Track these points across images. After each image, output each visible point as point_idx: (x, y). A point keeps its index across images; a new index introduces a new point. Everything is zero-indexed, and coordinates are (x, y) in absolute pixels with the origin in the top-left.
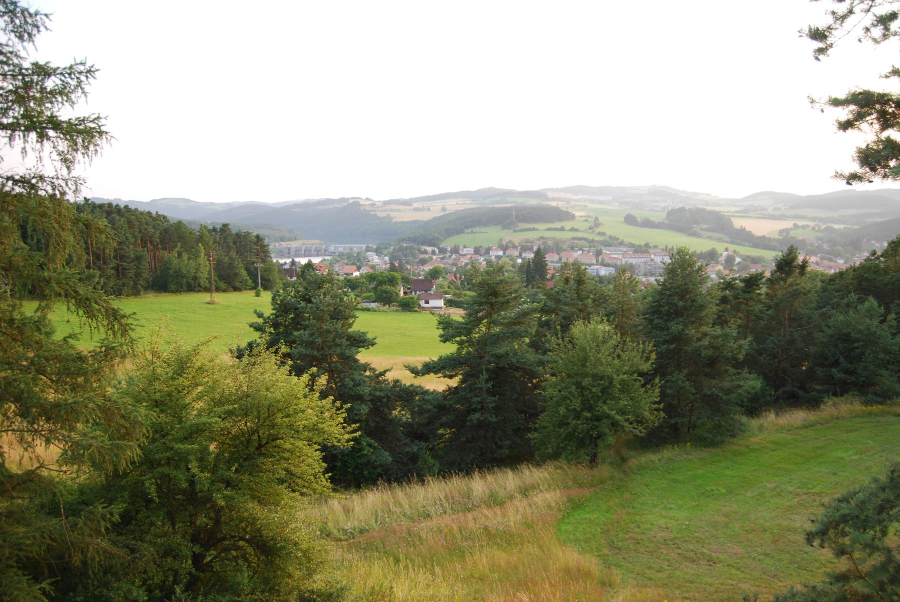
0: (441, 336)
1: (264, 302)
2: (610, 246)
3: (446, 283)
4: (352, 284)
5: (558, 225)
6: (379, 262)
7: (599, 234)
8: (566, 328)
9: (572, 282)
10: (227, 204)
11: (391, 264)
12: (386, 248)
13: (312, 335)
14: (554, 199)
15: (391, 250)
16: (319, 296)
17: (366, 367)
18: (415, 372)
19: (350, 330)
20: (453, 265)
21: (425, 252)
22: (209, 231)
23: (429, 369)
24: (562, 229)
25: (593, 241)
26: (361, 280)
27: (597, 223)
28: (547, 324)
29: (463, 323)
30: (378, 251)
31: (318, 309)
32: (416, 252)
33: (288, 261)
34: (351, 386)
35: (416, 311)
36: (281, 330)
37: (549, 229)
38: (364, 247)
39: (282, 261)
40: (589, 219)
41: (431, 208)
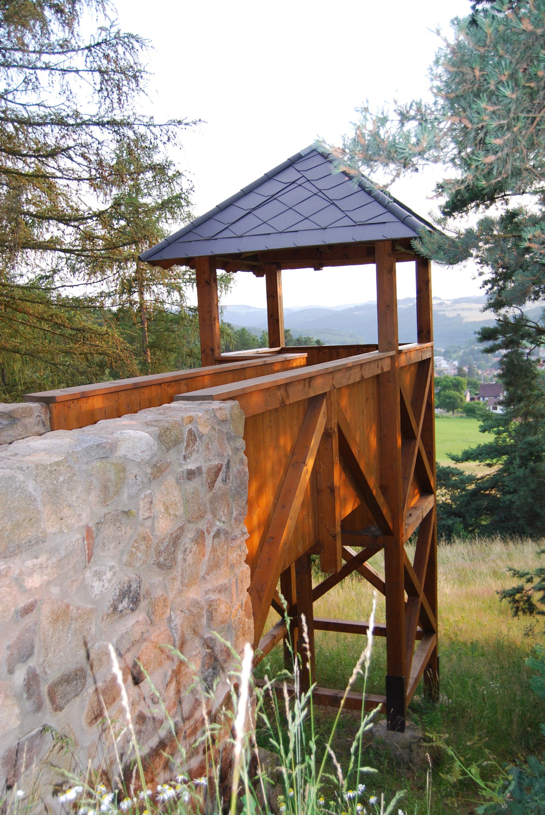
0: (481, 427)
11: (460, 369)
12: (455, 352)
15: (461, 353)
18: (456, 459)
23: (468, 456)
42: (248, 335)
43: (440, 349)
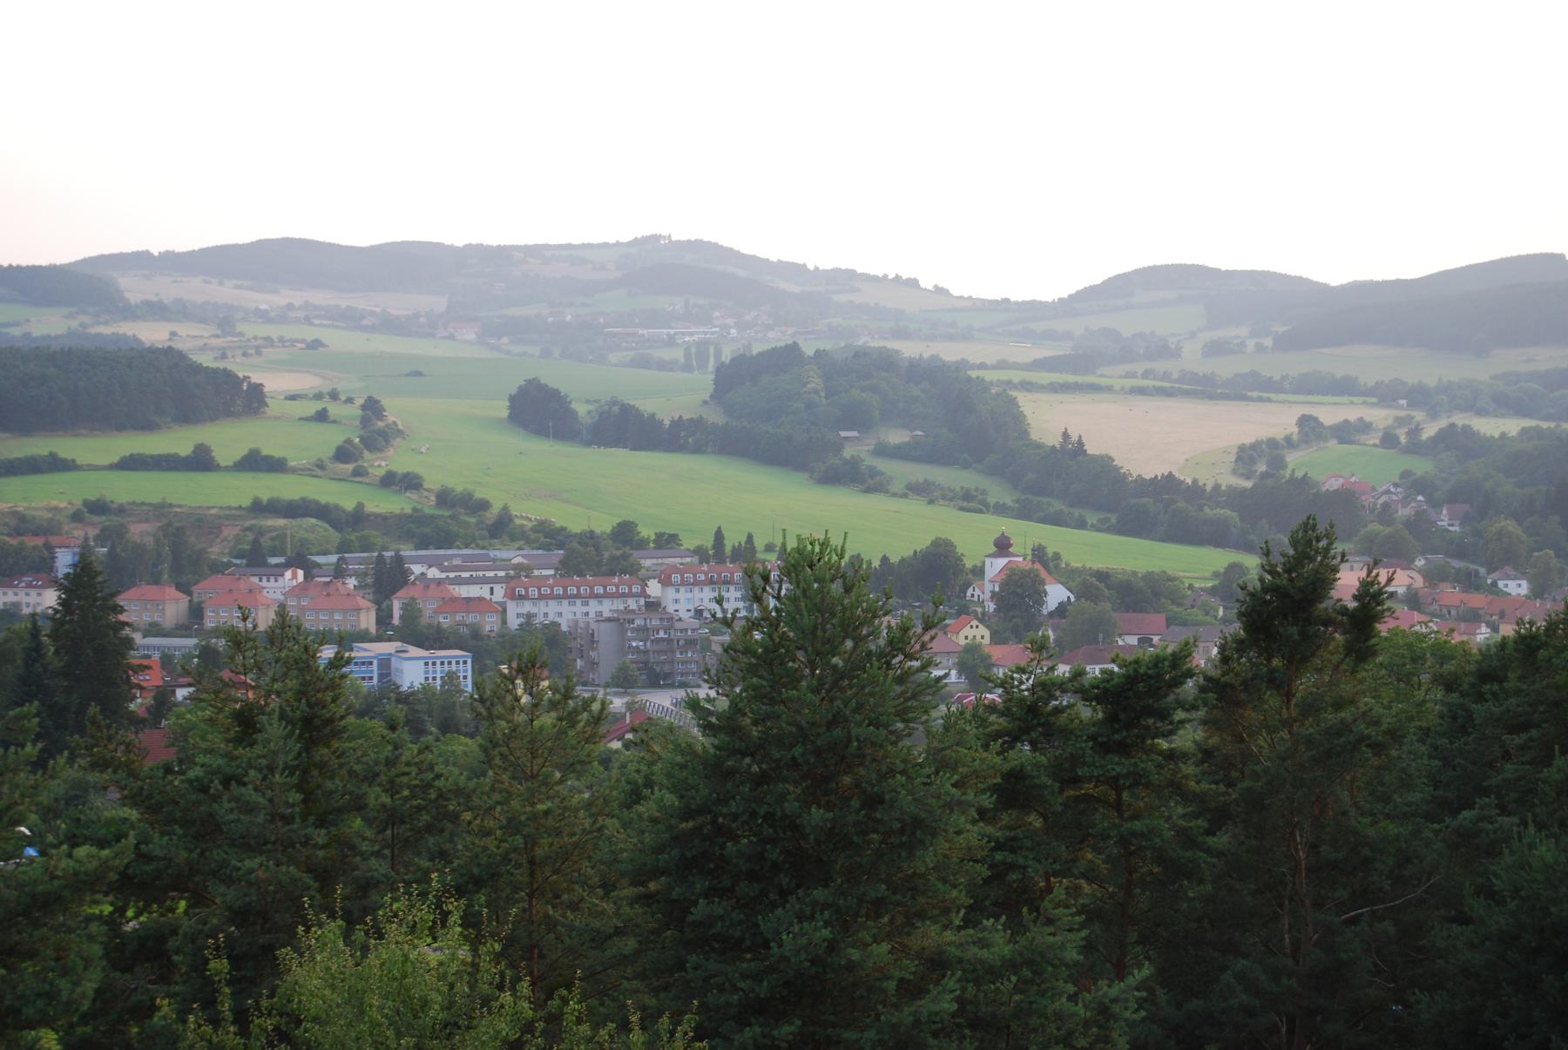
2: (446, 540)
5: (179, 441)
7: (389, 481)
8: (256, 964)
9: (274, 730)
14: (155, 310)
24: (201, 461)
25: (358, 518)
27: (375, 430)
28: (151, 952)
37: (132, 463)
40: (335, 410)
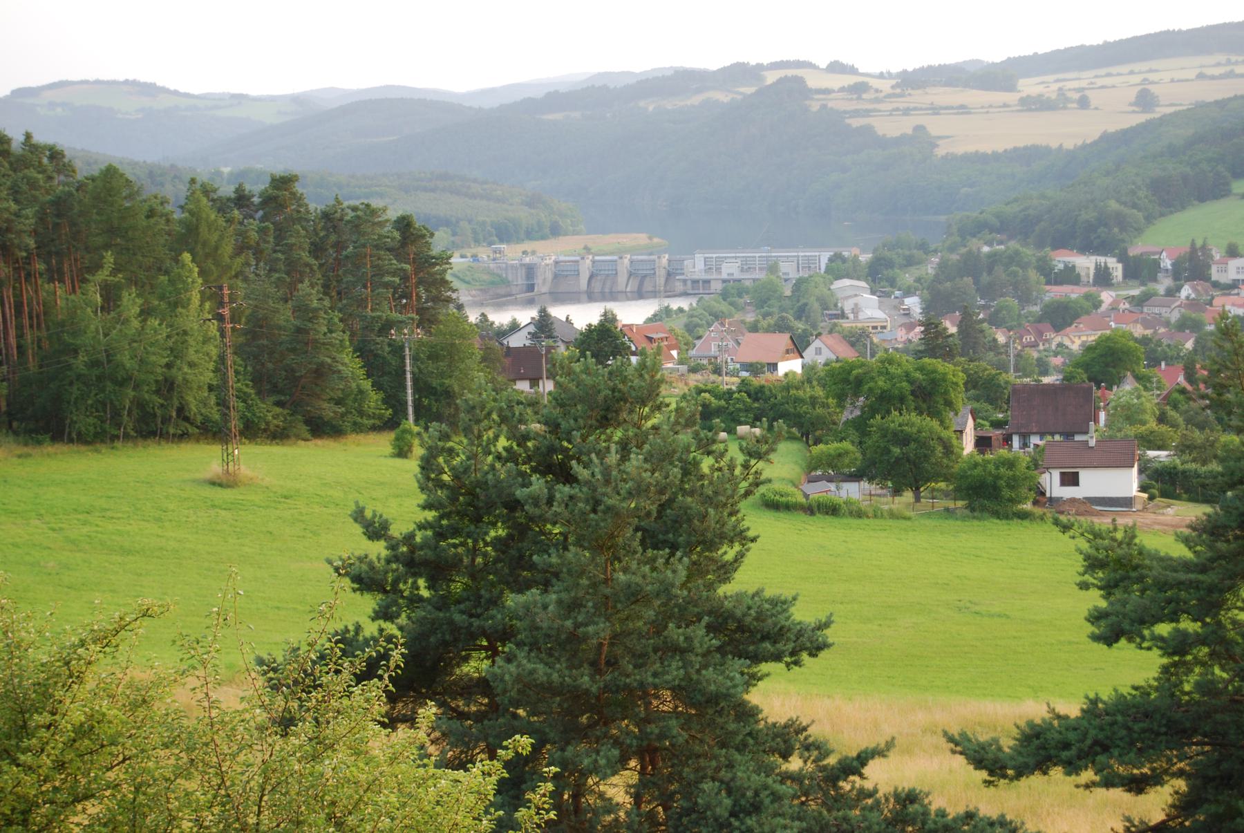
0: (1096, 617)
1: (375, 480)
3: (1150, 401)
4: (767, 407)
6: (882, 318)
10: (296, 99)
11: (932, 328)
12: (910, 262)
13: (572, 607)
15: (930, 269)
16: (602, 454)
17: (787, 738)
18: (990, 762)
19: (724, 590)
20: (1184, 325)
21: (1070, 276)
22: (222, 206)
26: (806, 393)
29: (1186, 566)
30: (879, 275)
31: (595, 504)
32: (1033, 275)
33: (525, 316)
34: (722, 812)
35: (1024, 516)
36: (457, 587)
38: (825, 257)
39: (500, 318)
41: (1094, 97)
42: (130, 197)
43: (855, 251)
